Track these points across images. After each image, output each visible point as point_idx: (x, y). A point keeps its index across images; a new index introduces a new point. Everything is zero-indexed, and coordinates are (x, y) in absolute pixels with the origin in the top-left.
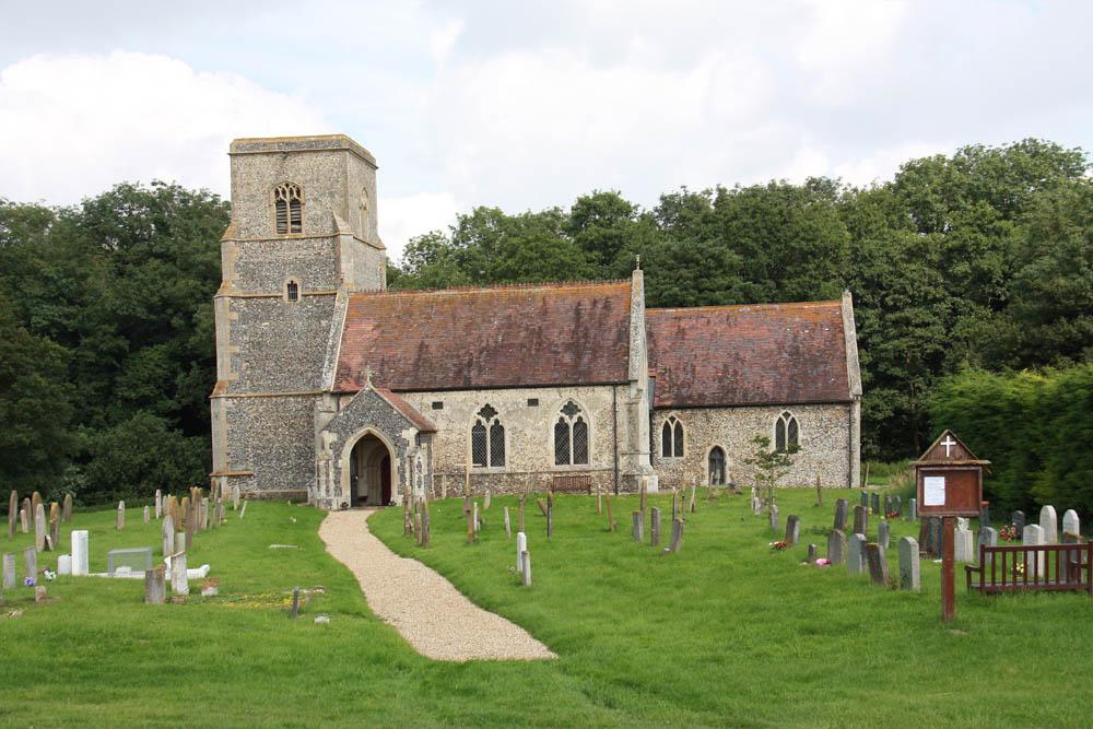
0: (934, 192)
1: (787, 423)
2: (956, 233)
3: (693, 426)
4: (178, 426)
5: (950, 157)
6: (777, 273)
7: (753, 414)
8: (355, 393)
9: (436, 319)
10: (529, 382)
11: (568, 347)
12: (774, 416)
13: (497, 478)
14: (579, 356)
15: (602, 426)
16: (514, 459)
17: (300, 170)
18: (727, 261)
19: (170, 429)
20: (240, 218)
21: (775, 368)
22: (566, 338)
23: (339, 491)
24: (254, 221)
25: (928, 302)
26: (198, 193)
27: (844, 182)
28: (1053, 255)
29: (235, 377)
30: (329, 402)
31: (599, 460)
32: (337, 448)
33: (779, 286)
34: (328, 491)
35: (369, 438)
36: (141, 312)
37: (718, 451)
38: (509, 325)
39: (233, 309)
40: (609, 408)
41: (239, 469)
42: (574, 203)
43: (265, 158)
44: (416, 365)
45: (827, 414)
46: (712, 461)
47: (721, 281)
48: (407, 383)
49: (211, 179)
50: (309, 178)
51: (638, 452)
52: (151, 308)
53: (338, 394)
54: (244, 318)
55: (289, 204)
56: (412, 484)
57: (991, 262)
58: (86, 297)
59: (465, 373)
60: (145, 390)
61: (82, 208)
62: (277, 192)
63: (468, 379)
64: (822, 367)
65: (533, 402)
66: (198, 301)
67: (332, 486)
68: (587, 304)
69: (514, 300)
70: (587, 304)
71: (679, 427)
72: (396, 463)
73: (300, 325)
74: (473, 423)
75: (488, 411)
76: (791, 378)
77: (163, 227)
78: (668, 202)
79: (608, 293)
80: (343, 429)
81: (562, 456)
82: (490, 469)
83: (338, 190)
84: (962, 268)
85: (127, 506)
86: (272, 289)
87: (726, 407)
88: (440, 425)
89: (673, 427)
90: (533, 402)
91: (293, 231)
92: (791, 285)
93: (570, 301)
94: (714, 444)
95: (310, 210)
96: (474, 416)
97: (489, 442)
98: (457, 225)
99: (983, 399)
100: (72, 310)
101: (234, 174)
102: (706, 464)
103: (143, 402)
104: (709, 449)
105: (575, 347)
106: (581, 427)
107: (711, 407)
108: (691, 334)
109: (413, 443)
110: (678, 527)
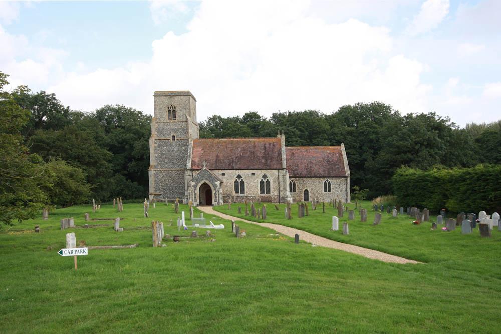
0: (351, 115)
1: (327, 183)
2: (362, 127)
3: (298, 183)
7: (317, 179)
11: (263, 157)
12: (324, 180)
13: (242, 198)
15: (275, 182)
16: (247, 192)
17: (176, 101)
18: (296, 133)
22: (262, 155)
23: (196, 200)
26: (129, 109)
27: (437, 114)
29: (156, 164)
30: (189, 172)
31: (274, 193)
32: (195, 187)
34: (192, 200)
35: (205, 184)
36: (116, 144)
37: (306, 191)
38: (244, 150)
39: (155, 143)
40: (277, 176)
41: (158, 193)
42: (244, 115)
43: (165, 97)
45: (339, 180)
46: (305, 194)
48: (214, 167)
50: (175, 104)
51: (286, 190)
52: (118, 142)
54: (159, 146)
55: (172, 112)
59: (232, 165)
62: (168, 108)
63: (232, 166)
65: (253, 174)
66: (133, 141)
67: (193, 199)
69: (245, 143)
70: (267, 145)
72: (213, 192)
73: (176, 149)
74: (234, 180)
76: (328, 169)
78: (275, 116)
81: (262, 192)
82: (240, 195)
86: (167, 137)
87: (309, 177)
88: (224, 180)
89: (292, 183)
90: (253, 174)
91: (173, 119)
92: (314, 141)
93: (262, 143)
94: (306, 189)
95: (179, 113)
96: (235, 178)
97: (240, 186)
98: (207, 120)
101: (155, 102)
102: (303, 195)
104: (304, 190)
105: (266, 157)
106: (268, 182)
107: (304, 177)
109: (218, 186)
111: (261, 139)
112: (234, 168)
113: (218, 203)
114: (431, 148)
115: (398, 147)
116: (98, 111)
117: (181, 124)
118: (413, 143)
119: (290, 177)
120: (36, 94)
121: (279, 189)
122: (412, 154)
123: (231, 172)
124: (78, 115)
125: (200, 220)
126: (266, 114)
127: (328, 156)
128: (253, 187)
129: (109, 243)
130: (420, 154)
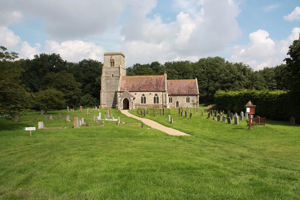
0: (205, 63)
1: (188, 98)
3: (174, 98)
4: (93, 96)
5: (206, 58)
6: (183, 75)
8: (123, 92)
9: (135, 80)
10: (150, 91)
14: (157, 87)
16: (147, 103)
17: (114, 57)
18: (176, 73)
19: (92, 97)
20: (105, 65)
21: (186, 89)
22: (155, 84)
23: (121, 107)
24: (107, 65)
25: (205, 80)
27: (243, 63)
28: (224, 74)
31: (160, 103)
32: (121, 100)
33: (183, 77)
38: (146, 82)
42: (151, 63)
44: (132, 88)
46: (177, 103)
47: (175, 76)
49: (99, 59)
50: (113, 58)
52: (89, 78)
53: (120, 92)
54: (105, 80)
55: (112, 63)
56: (132, 107)
57: (214, 74)
58: (80, 76)
60: (88, 90)
61: (79, 63)
63: (140, 90)
64: (193, 89)
65: (150, 94)
66: (96, 77)
67: (120, 106)
68: (158, 79)
69: (147, 78)
70: (158, 79)
71: (172, 98)
72: (130, 103)
74: (141, 97)
75: (143, 95)
77: (90, 65)
79: (161, 77)
80: (122, 97)
81: (155, 102)
82: (144, 104)
83: (120, 60)
84: (209, 75)
85: (74, 110)
88: (136, 97)
90: (150, 94)
96: (141, 96)
97: (144, 100)
98: (133, 66)
99: (224, 95)
100: (78, 78)
101: (104, 58)
102: (176, 104)
103: (87, 92)
104: (176, 102)
105: (157, 85)
106: (158, 98)
108: (173, 84)
109: (132, 100)
110: (191, 114)
111: (155, 76)
112: (141, 90)
113: (132, 109)
114: (240, 80)
115: (224, 80)
116: (80, 62)
117: (116, 69)
118: (231, 78)
119: (169, 95)
120: (51, 55)
121: (163, 101)
122: (231, 84)
123: (139, 93)
124: (71, 64)
125: (107, 117)
126: (162, 63)
127: (189, 85)
128: (150, 100)
129: (57, 127)
130: (234, 83)
